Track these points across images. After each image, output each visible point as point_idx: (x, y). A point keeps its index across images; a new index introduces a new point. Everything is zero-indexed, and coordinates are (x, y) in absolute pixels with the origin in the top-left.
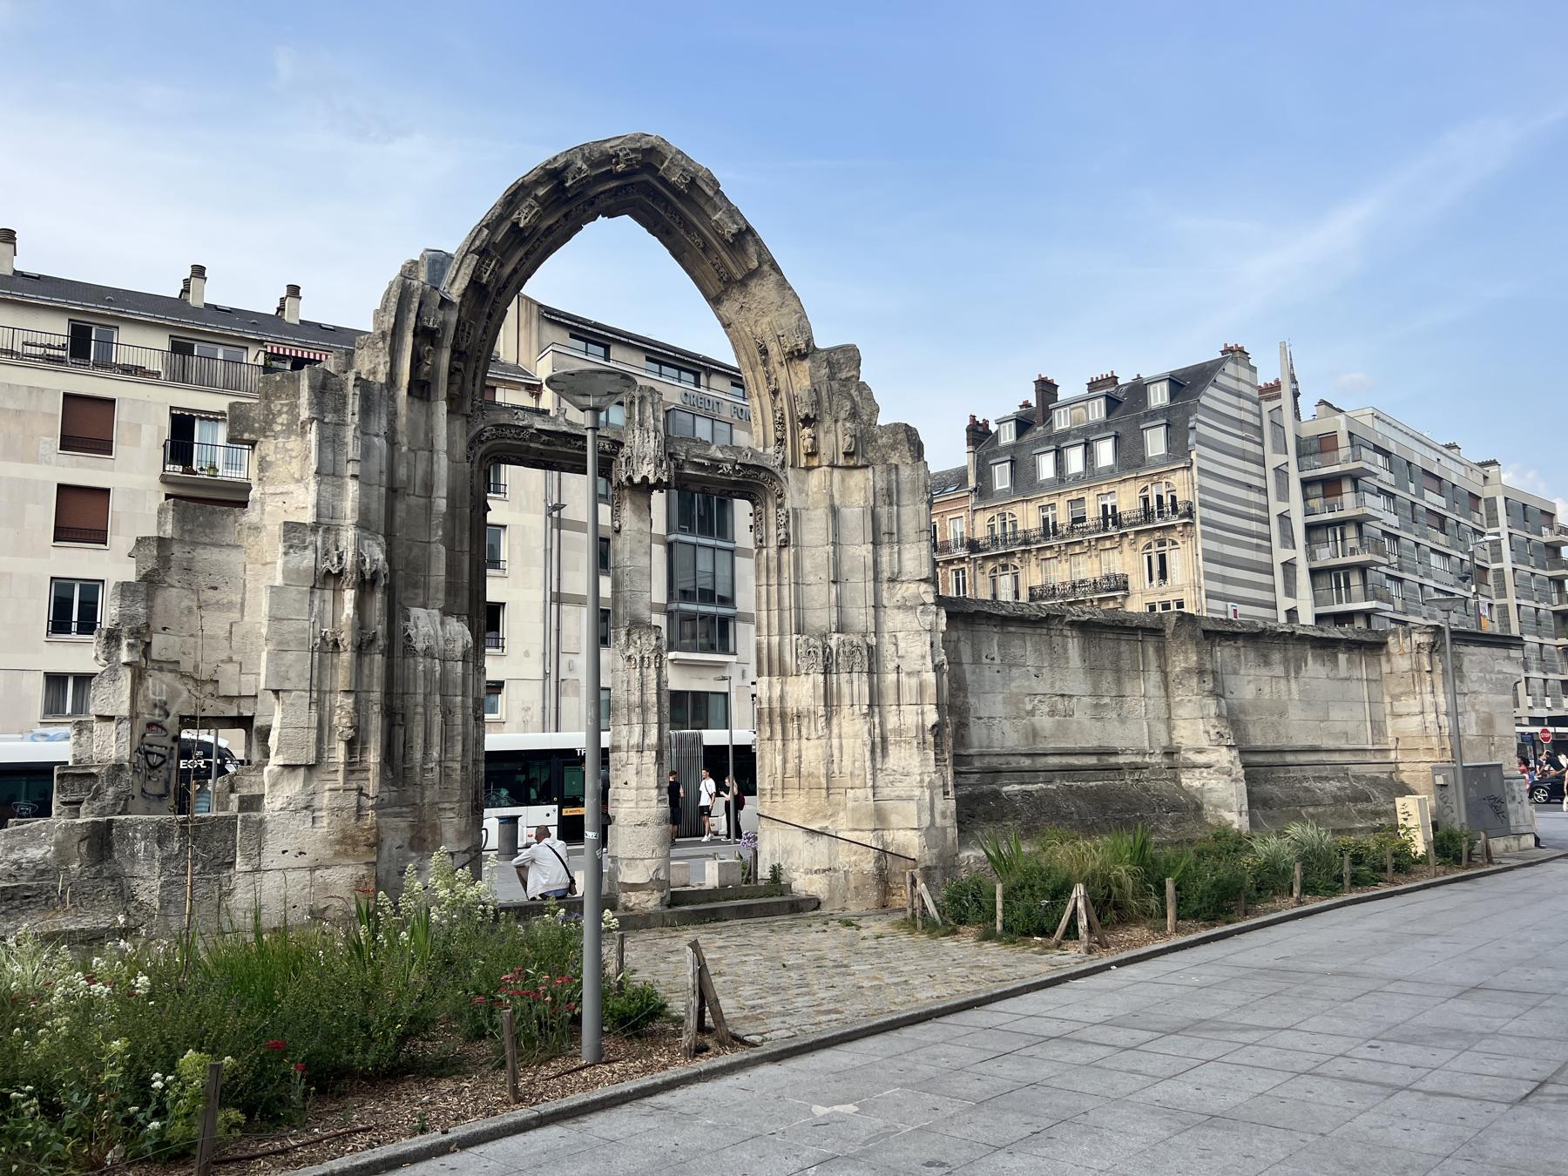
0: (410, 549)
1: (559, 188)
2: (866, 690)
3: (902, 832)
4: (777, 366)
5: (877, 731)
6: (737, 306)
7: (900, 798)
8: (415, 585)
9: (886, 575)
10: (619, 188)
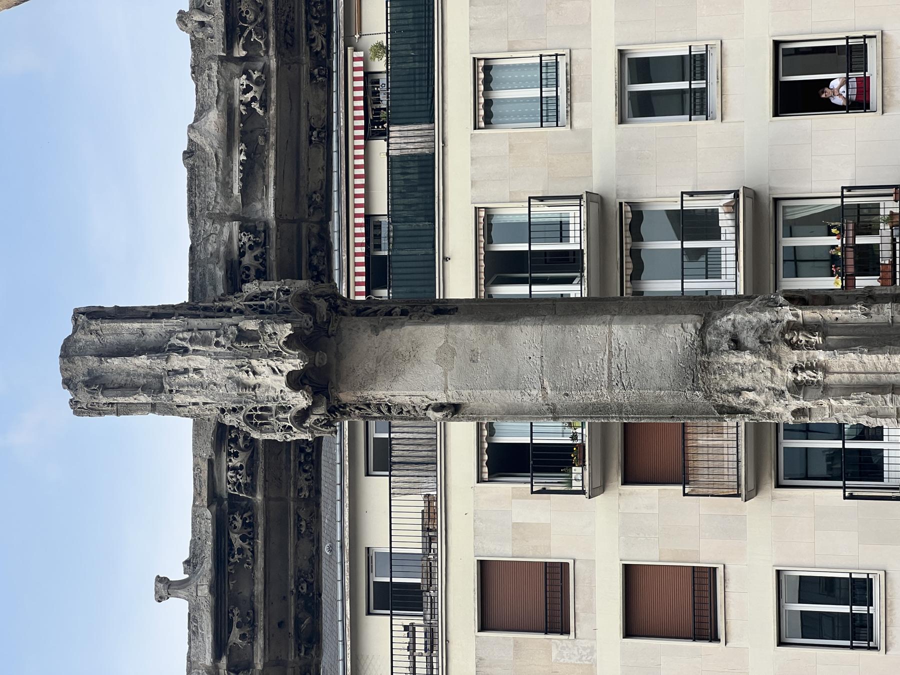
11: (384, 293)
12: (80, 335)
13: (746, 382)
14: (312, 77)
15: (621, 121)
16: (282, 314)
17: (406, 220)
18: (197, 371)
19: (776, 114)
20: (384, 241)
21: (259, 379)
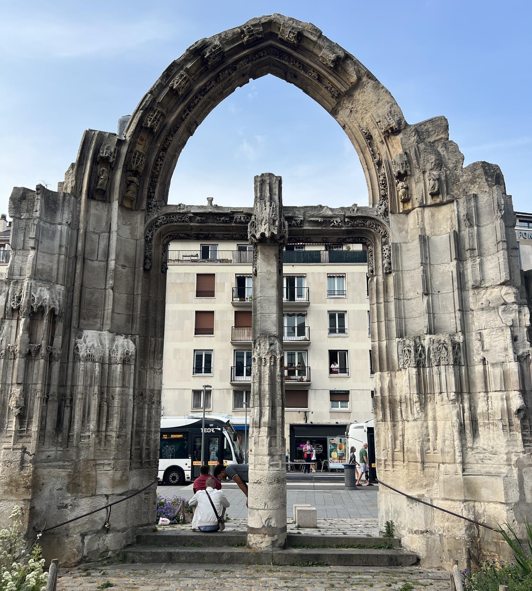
0: (92, 294)
1: (204, 62)
2: (452, 380)
3: (492, 505)
4: (379, 145)
5: (467, 414)
7: (489, 474)
8: (95, 317)
9: (470, 283)
11: (284, 249)
12: (275, 178)
13: (262, 347)
14: (340, 239)
15: (328, 311)
16: (279, 231)
17: (303, 255)
18: (266, 209)
19: (329, 350)
20: (298, 250)
21: (263, 225)
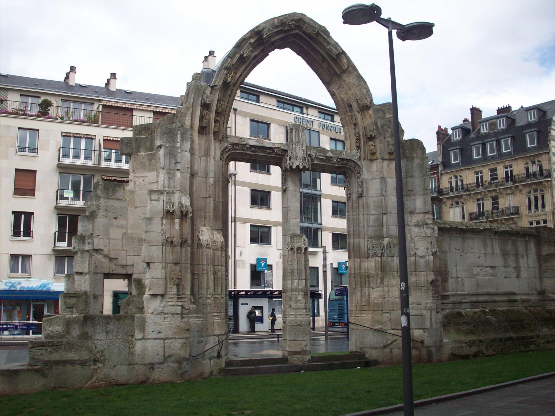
4: (356, 113)
6: (337, 86)
10: (285, 37)
